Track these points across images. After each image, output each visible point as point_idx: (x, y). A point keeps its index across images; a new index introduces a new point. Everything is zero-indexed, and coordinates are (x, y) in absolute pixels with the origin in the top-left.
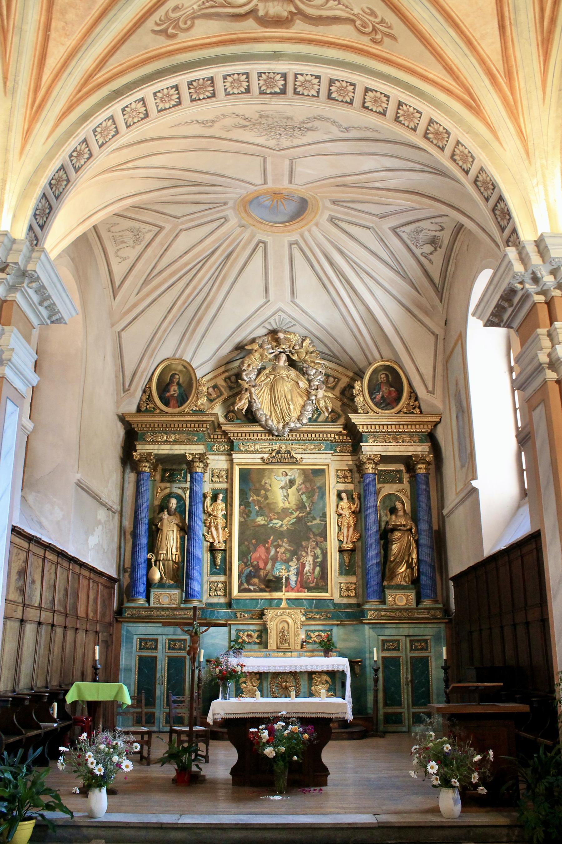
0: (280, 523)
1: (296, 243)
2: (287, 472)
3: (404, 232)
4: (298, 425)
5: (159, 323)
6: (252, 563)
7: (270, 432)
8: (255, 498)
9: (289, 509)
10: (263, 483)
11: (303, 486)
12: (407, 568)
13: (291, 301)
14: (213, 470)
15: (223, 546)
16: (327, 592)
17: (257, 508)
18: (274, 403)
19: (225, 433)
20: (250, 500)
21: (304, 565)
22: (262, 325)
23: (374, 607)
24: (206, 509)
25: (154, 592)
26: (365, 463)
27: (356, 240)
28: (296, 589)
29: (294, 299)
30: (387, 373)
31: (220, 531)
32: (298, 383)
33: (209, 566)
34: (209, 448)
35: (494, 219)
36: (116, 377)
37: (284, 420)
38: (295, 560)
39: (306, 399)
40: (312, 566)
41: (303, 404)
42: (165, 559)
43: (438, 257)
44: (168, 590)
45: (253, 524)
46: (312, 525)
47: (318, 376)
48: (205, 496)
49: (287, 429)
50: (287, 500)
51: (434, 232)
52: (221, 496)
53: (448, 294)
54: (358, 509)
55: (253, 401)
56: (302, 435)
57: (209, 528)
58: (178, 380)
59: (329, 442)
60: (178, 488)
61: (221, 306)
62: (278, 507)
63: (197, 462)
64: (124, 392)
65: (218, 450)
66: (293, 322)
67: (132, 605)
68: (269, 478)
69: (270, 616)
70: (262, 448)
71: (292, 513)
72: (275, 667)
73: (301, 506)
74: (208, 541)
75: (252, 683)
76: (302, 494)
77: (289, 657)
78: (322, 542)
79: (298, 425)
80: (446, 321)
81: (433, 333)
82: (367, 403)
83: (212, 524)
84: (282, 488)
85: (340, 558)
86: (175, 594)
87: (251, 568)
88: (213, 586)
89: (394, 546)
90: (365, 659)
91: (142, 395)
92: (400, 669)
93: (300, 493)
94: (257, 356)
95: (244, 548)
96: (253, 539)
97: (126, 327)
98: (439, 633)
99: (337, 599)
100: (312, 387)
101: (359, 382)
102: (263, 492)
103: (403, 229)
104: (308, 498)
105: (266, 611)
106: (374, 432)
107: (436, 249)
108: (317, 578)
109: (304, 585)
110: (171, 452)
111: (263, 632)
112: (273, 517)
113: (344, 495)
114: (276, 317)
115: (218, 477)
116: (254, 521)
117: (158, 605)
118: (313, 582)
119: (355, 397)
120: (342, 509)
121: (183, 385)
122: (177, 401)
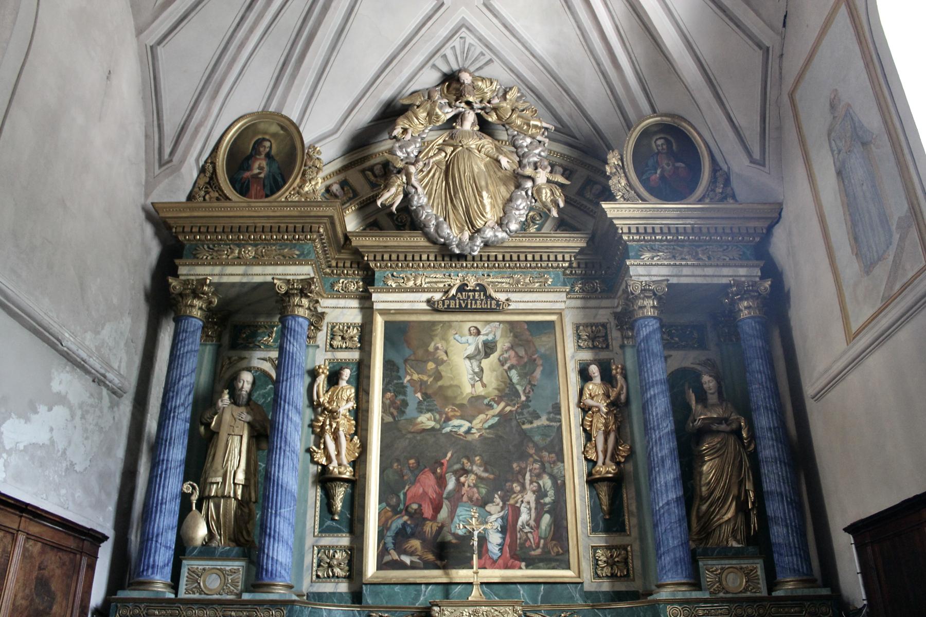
0: (466, 425)
2: (479, 327)
4: (501, 235)
5: (232, 30)
6: (406, 508)
9: (484, 397)
10: (431, 348)
11: (512, 353)
14: (333, 327)
15: (347, 474)
16: (569, 568)
17: (419, 395)
19: (357, 253)
21: (517, 512)
23: (680, 596)
25: (188, 565)
28: (501, 561)
32: (499, 161)
33: (318, 514)
34: (328, 285)
36: (147, 136)
37: (473, 226)
38: (497, 500)
40: (533, 515)
41: (508, 196)
42: (219, 495)
44: (220, 563)
45: (412, 429)
47: (536, 148)
48: (314, 374)
49: (479, 242)
50: (481, 380)
52: (347, 373)
54: (623, 397)
58: (267, 150)
60: (264, 359)
62: (462, 393)
64: (161, 166)
65: (345, 288)
66: (489, 55)
67: (135, 594)
71: (490, 406)
73: (508, 392)
74: (317, 463)
76: (510, 368)
79: (501, 235)
80: (785, 16)
81: (759, 45)
83: (328, 427)
84: (469, 358)
85: (591, 497)
86: (233, 572)
87: (406, 518)
91: (198, 176)
93: (506, 367)
96: (411, 458)
97: (165, 36)
99: (589, 583)
102: (431, 366)
104: (522, 376)
105: (436, 609)
106: (651, 240)
108: (545, 539)
110: (245, 280)
113: (594, 370)
114: (456, 42)
115: (343, 338)
116: (412, 421)
117: (197, 596)
118: (538, 547)
119: (609, 178)
121: (277, 158)
122: (264, 186)
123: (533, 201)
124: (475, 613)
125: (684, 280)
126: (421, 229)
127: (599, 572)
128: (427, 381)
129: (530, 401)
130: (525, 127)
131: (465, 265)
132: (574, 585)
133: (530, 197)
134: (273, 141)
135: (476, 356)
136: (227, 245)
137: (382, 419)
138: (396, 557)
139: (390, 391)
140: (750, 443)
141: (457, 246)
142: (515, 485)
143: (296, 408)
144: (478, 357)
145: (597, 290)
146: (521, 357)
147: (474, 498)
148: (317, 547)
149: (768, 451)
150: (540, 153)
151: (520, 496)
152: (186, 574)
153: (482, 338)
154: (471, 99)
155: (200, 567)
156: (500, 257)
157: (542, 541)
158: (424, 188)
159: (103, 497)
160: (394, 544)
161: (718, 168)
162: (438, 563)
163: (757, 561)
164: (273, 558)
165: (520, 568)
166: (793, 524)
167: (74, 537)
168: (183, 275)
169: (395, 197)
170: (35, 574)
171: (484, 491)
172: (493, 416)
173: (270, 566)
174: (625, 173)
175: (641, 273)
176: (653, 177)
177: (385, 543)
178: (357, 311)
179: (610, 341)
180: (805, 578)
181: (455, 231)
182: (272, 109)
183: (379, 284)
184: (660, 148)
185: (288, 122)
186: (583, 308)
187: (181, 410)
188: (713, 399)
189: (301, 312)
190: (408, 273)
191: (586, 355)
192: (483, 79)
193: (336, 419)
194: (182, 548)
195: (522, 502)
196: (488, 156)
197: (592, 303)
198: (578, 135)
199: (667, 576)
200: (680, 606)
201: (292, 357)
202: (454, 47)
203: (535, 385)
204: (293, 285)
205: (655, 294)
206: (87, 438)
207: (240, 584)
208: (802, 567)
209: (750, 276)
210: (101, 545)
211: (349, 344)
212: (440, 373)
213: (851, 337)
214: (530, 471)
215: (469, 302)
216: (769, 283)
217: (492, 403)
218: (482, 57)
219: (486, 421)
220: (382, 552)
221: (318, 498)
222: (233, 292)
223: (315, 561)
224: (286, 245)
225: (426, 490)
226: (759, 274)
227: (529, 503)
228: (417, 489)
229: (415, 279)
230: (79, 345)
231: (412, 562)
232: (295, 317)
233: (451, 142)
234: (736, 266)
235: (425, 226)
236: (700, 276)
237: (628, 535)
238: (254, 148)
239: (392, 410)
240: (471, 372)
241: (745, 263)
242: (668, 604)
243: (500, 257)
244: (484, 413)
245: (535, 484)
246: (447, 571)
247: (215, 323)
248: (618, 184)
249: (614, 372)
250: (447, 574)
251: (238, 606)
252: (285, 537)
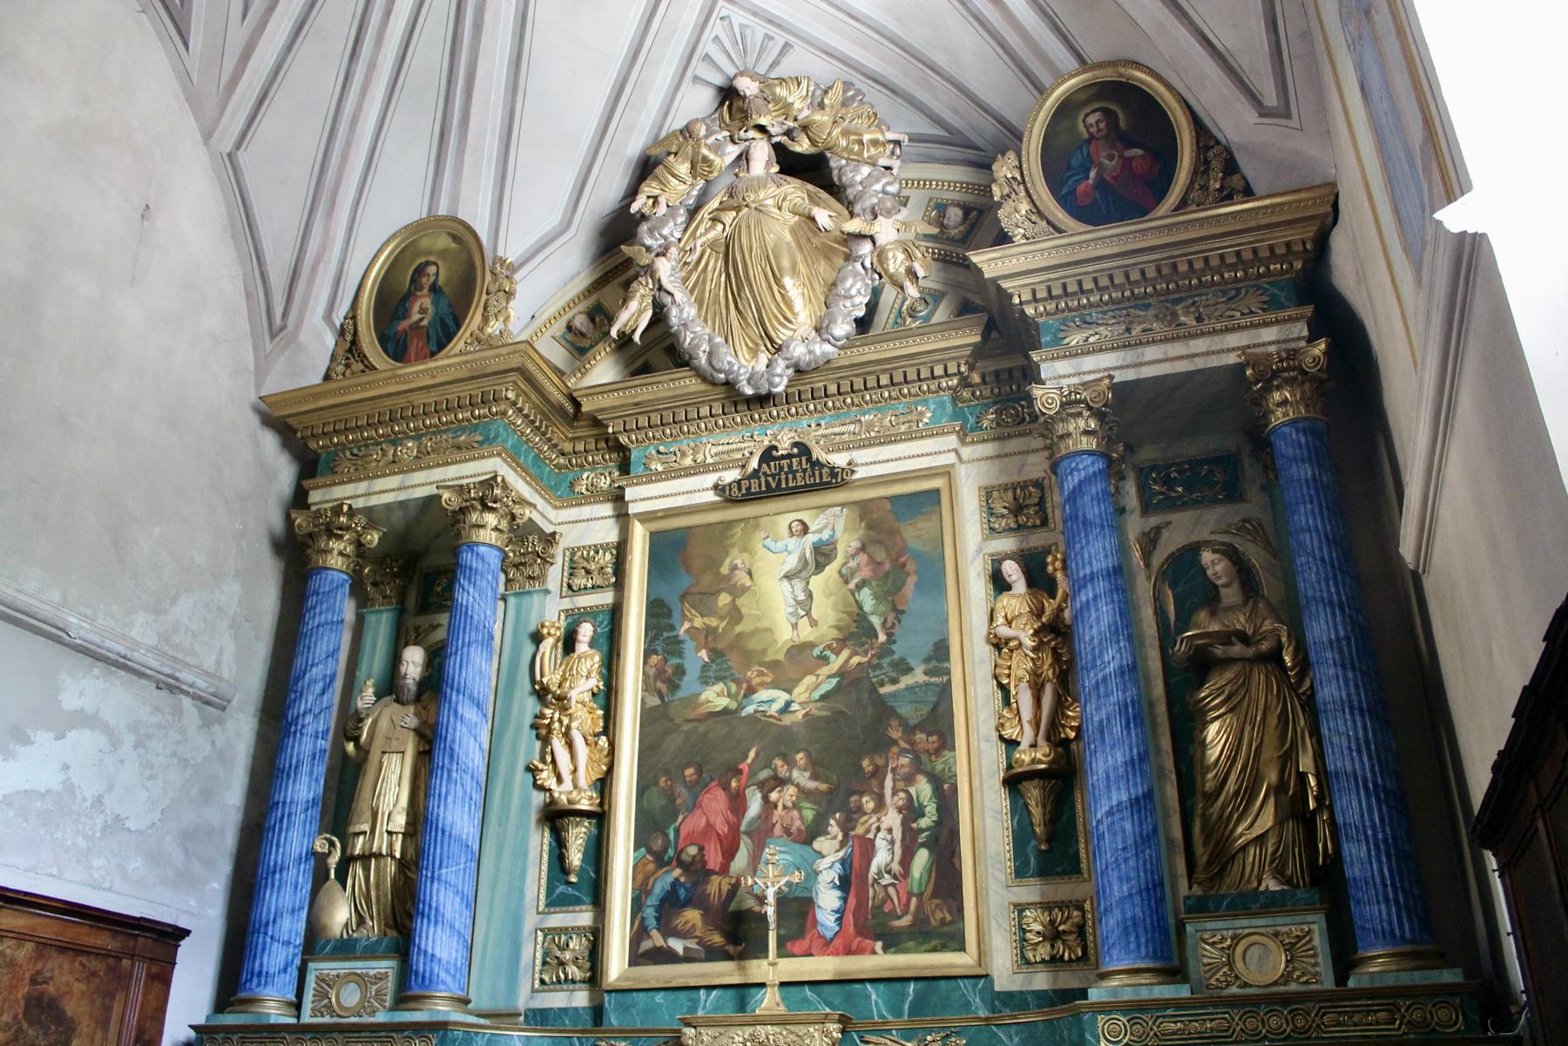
0: (782, 697)
2: (806, 520)
6: (679, 853)
9: (811, 645)
10: (725, 570)
11: (863, 558)
12: (1279, 822)
14: (573, 554)
16: (962, 949)
17: (704, 654)
21: (868, 849)
23: (1127, 995)
24: (538, 677)
28: (838, 942)
31: (582, 749)
32: (813, 219)
33: (544, 875)
36: (248, 295)
38: (834, 828)
44: (360, 964)
46: (893, 695)
49: (780, 366)
50: (808, 613)
52: (586, 631)
55: (668, 299)
57: (546, 741)
58: (432, 279)
62: (775, 641)
64: (273, 336)
66: (780, 38)
68: (745, 549)
71: (824, 660)
73: (856, 630)
74: (542, 788)
76: (859, 587)
83: (557, 725)
86: (379, 978)
87: (677, 872)
89: (1213, 729)
93: (852, 585)
95: (656, 801)
96: (688, 766)
99: (1005, 973)
102: (724, 599)
105: (690, 1032)
108: (920, 895)
110: (402, 496)
112: (756, 681)
113: (1011, 569)
114: (716, 28)
116: (693, 700)
117: (327, 1019)
118: (906, 912)
119: (999, 205)
121: (446, 290)
122: (428, 338)
123: (877, 276)
124: (753, 1037)
126: (687, 364)
127: (1030, 955)
128: (717, 627)
129: (895, 642)
130: (856, 148)
131: (775, 413)
132: (972, 981)
133: (870, 272)
134: (440, 263)
135: (800, 572)
136: (378, 444)
137: (643, 702)
139: (655, 652)
142: (865, 799)
143: (471, 697)
144: (804, 574)
145: (1024, 418)
146: (880, 564)
147: (794, 829)
148: (542, 930)
150: (884, 187)
151: (874, 819)
152: (313, 985)
153: (811, 538)
154: (763, 121)
155: (334, 973)
156: (833, 389)
157: (914, 901)
158: (692, 292)
159: (196, 867)
160: (658, 919)
161: (1212, 143)
162: (730, 948)
163: (1310, 918)
164: (426, 952)
165: (874, 952)
166: (1380, 836)
167: (110, 930)
168: (315, 504)
169: (639, 316)
170: (24, 990)
171: (809, 814)
172: (830, 677)
173: (421, 965)
175: (1062, 373)
176: (1082, 187)
179: (1049, 511)
180: (1407, 948)
181: (744, 354)
182: (442, 211)
183: (637, 469)
184: (1093, 130)
185: (461, 228)
186: (998, 456)
187: (308, 719)
189: (488, 536)
190: (685, 444)
192: (782, 80)
193: (566, 709)
194: (314, 943)
195: (878, 829)
196: (795, 214)
197: (1014, 445)
198: (979, 142)
199: (1111, 956)
200: (1125, 1016)
201: (466, 613)
202: (716, 37)
203: (903, 612)
204: (469, 492)
205: (1090, 408)
206: (151, 777)
207: (388, 998)
208: (1401, 925)
209: (1284, 341)
210: (182, 943)
211: (598, 581)
214: (893, 770)
215: (783, 477)
216: (1323, 346)
217: (828, 653)
218: (771, 44)
219: (818, 686)
221: (546, 848)
222: (398, 519)
223: (539, 955)
224: (463, 429)
225: (712, 820)
226: (1305, 333)
227: (890, 831)
228: (695, 822)
229: (695, 450)
230: (104, 634)
231: (686, 949)
232: (472, 546)
234: (1253, 326)
236: (1181, 358)
237: (1085, 881)
238: (413, 280)
239: (659, 685)
240: (792, 602)
242: (1101, 1012)
243: (833, 389)
244: (811, 673)
245: (902, 795)
246: (743, 963)
247: (395, 575)
248: (1014, 215)
249: (1050, 568)
250: (742, 969)
251: (368, 1034)
252: (448, 916)
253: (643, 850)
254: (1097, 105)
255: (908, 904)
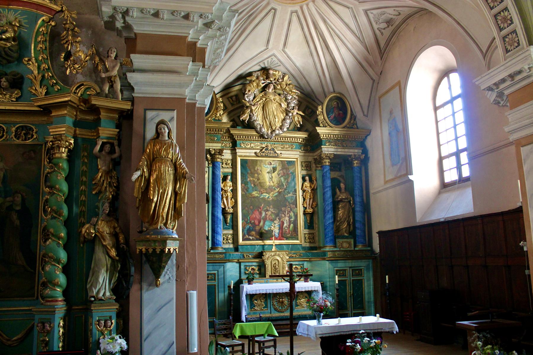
0: (268, 195)
1: (296, 12)
3: (372, 13)
4: (281, 132)
6: (250, 222)
7: (262, 136)
8: (251, 179)
11: (282, 172)
13: (282, 50)
17: (253, 185)
18: (265, 117)
19: (231, 136)
20: (248, 180)
21: (283, 223)
22: (259, 64)
26: (324, 159)
27: (337, 14)
28: (278, 238)
29: (285, 48)
30: (338, 102)
32: (281, 105)
35: (494, 21)
37: (272, 129)
38: (277, 219)
39: (285, 115)
40: (288, 223)
41: (283, 118)
43: (387, 33)
47: (294, 100)
49: (274, 135)
50: (272, 180)
51: (392, 16)
52: (229, 177)
53: (387, 55)
54: (315, 187)
56: (282, 138)
59: (298, 144)
61: (237, 49)
62: (266, 185)
63: (217, 155)
68: (260, 166)
69: (267, 256)
70: (255, 146)
71: (275, 189)
72: (276, 289)
73: (280, 185)
75: (261, 300)
76: (281, 177)
77: (280, 282)
78: (294, 208)
80: (381, 72)
81: (372, 79)
82: (325, 120)
83: (224, 196)
84: (268, 173)
85: (304, 218)
88: (225, 237)
90: (326, 282)
92: (346, 288)
93: (280, 176)
94: (255, 84)
96: (251, 206)
98: (369, 265)
100: (290, 107)
101: (321, 106)
102: (256, 175)
103: (372, 11)
104: (285, 179)
105: (264, 253)
107: (388, 26)
109: (282, 235)
111: (262, 267)
113: (307, 178)
114: (269, 60)
115: (226, 164)
118: (289, 234)
119: (318, 116)
120: (306, 187)
125: (338, 153)
137: (241, 193)
138: (248, 237)
140: (353, 205)
141: (266, 135)
149: (358, 208)
162: (260, 239)
172: (276, 193)
174: (323, 114)
177: (244, 233)
178: (230, 154)
180: (364, 245)
184: (335, 105)
188: (343, 190)
191: (304, 172)
197: (307, 154)
198: (304, 89)
205: (329, 157)
212: (259, 178)
213: (386, 182)
219: (274, 194)
220: (244, 236)
226: (361, 152)
227: (287, 220)
233: (265, 97)
235: (256, 128)
239: (244, 190)
241: (357, 148)
250: (263, 242)
253: (243, 221)
254: (336, 101)
255: (289, 233)
